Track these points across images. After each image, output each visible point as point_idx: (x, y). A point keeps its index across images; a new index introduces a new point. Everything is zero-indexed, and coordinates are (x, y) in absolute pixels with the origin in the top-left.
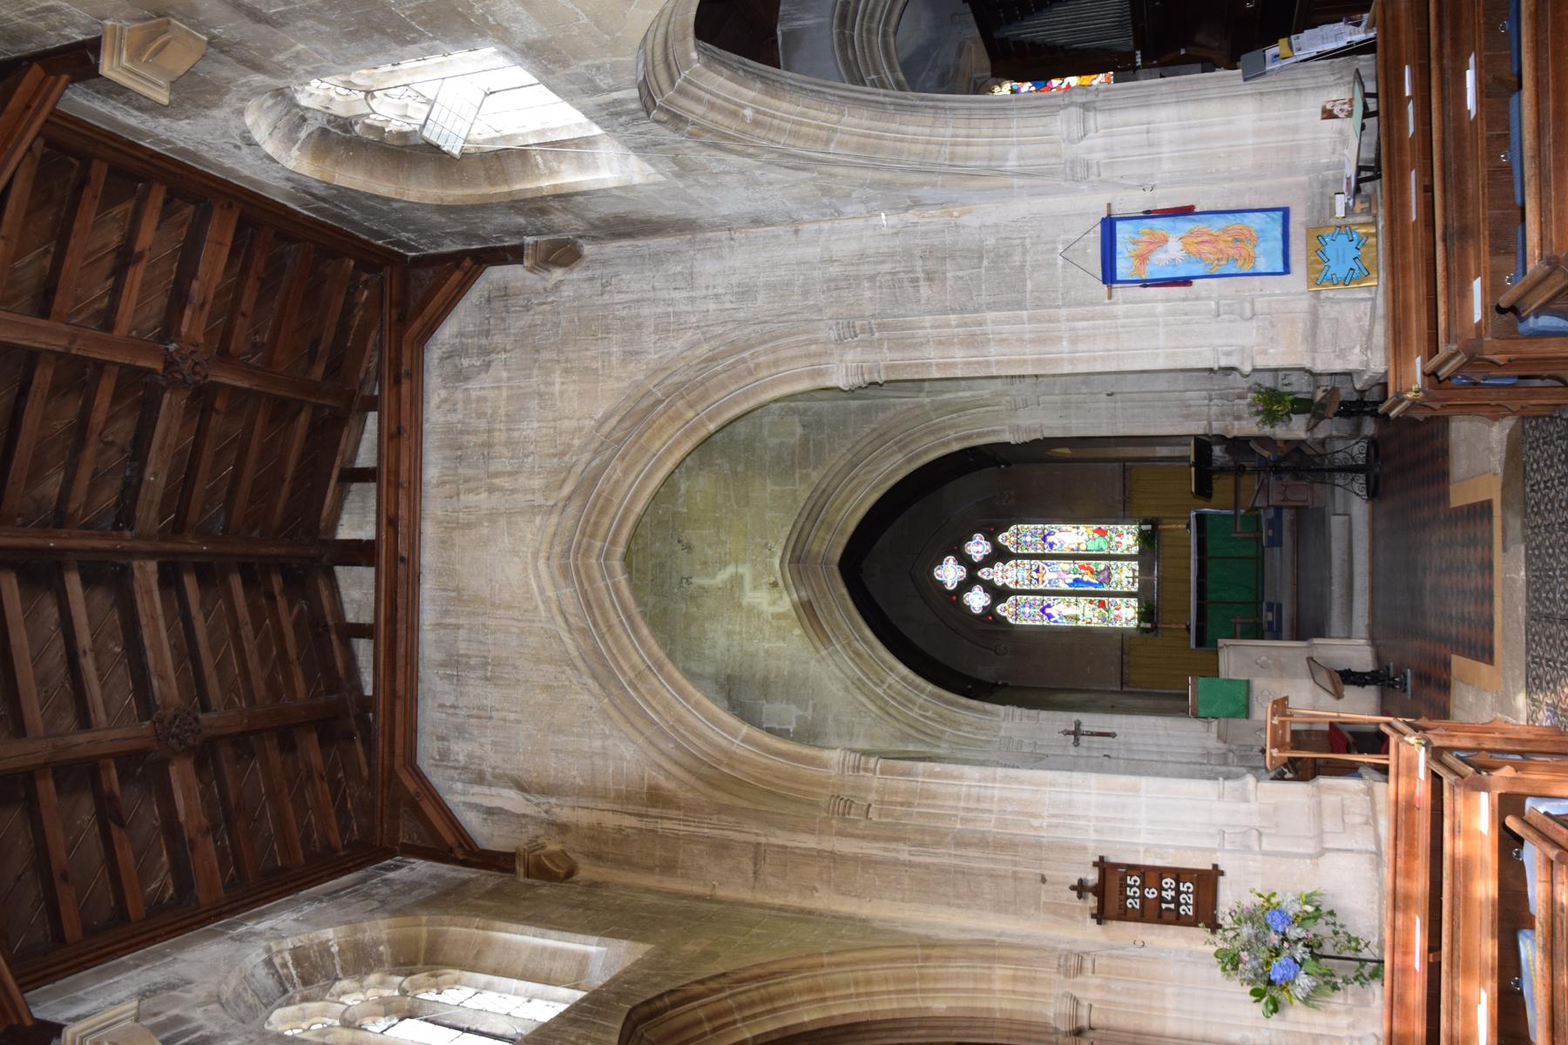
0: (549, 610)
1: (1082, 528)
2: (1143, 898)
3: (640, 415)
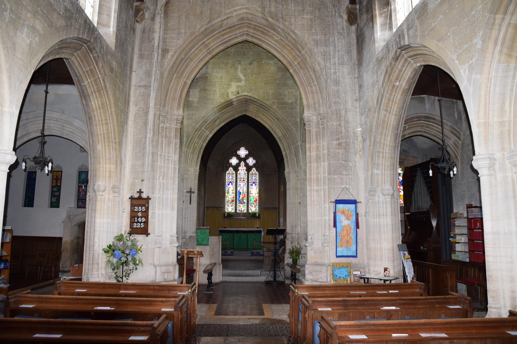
0: (229, 13)
1: (257, 195)
2: (138, 212)
3: (296, 46)
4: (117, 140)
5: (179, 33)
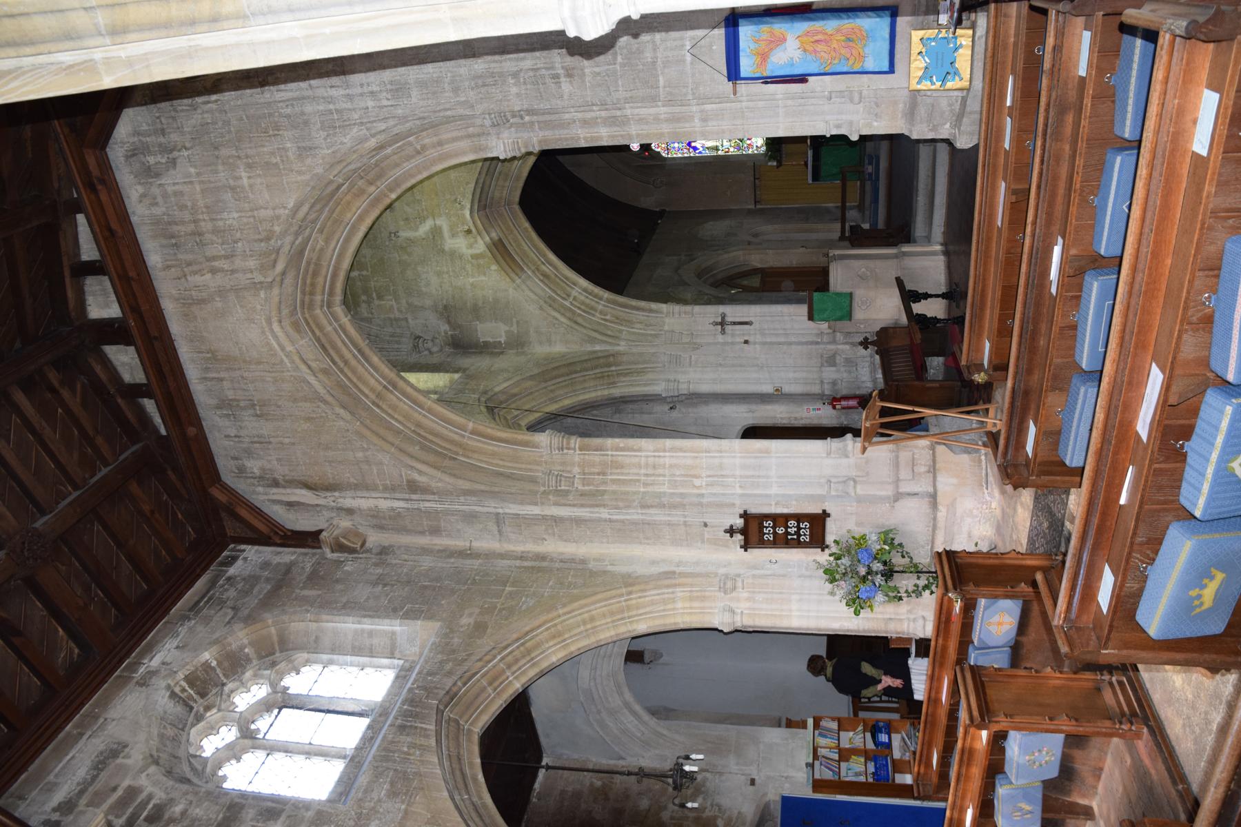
0: (293, 362)
2: (775, 533)
3: (327, 198)
4: (624, 590)
5: (367, 462)
